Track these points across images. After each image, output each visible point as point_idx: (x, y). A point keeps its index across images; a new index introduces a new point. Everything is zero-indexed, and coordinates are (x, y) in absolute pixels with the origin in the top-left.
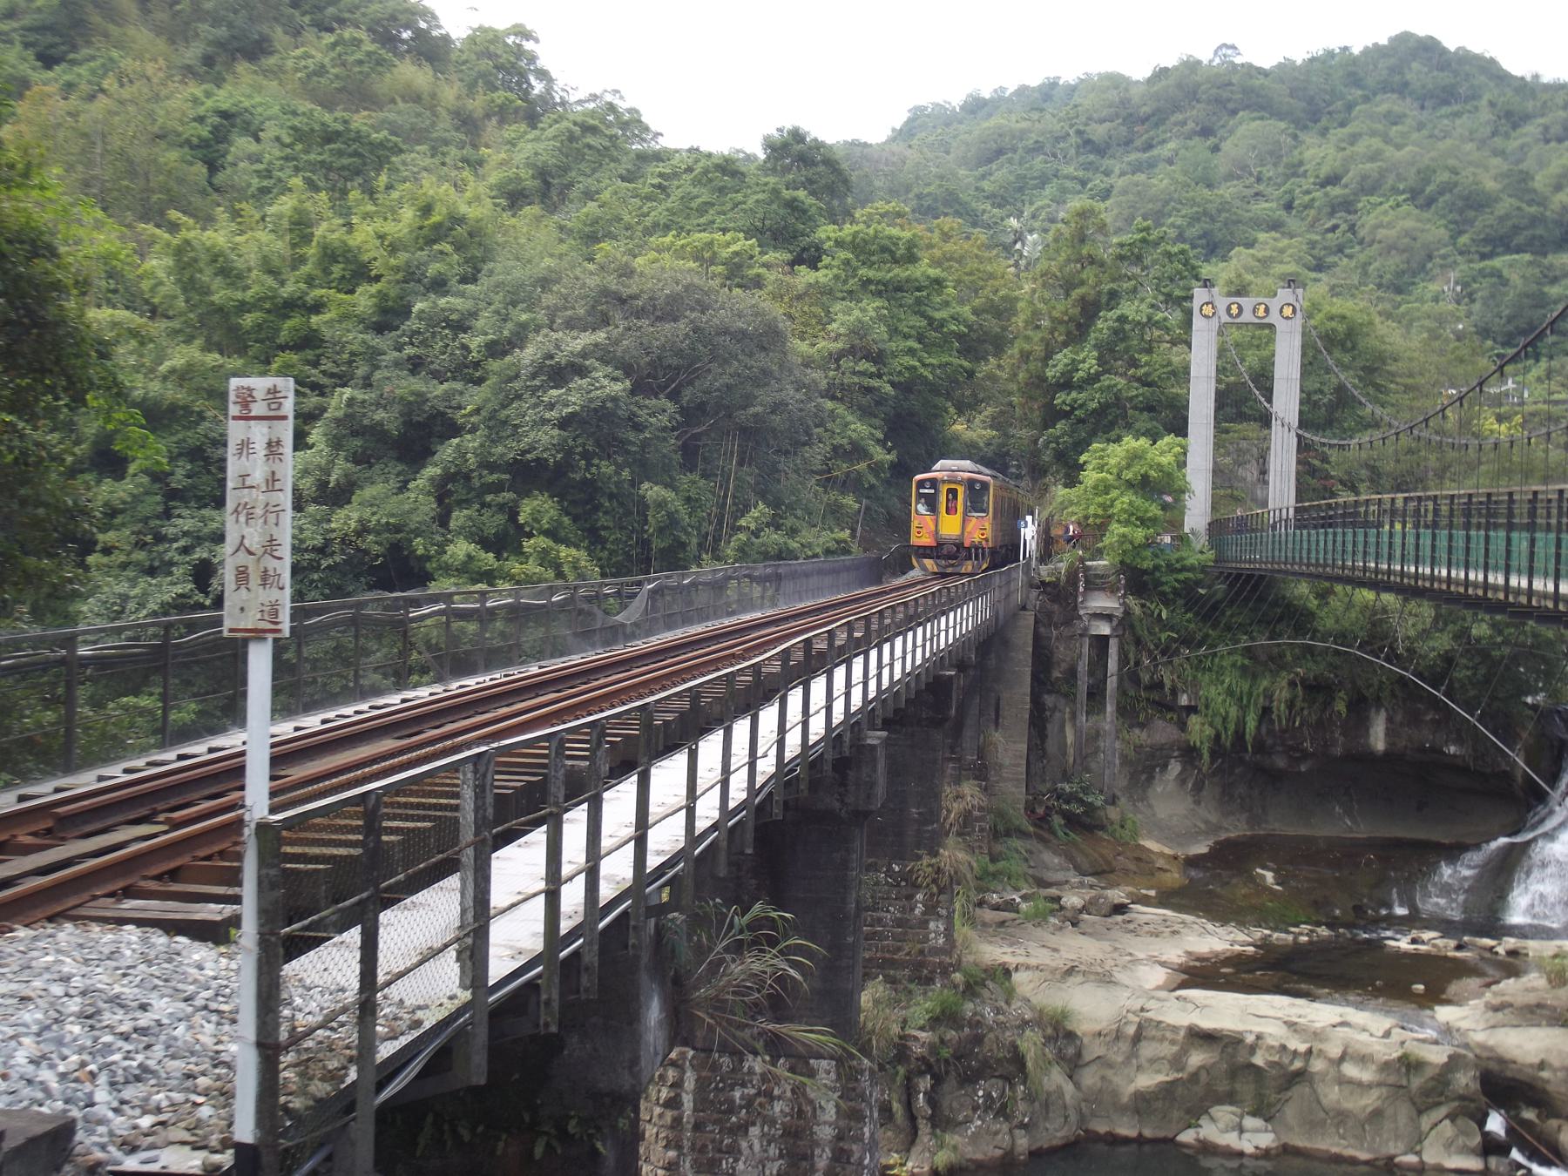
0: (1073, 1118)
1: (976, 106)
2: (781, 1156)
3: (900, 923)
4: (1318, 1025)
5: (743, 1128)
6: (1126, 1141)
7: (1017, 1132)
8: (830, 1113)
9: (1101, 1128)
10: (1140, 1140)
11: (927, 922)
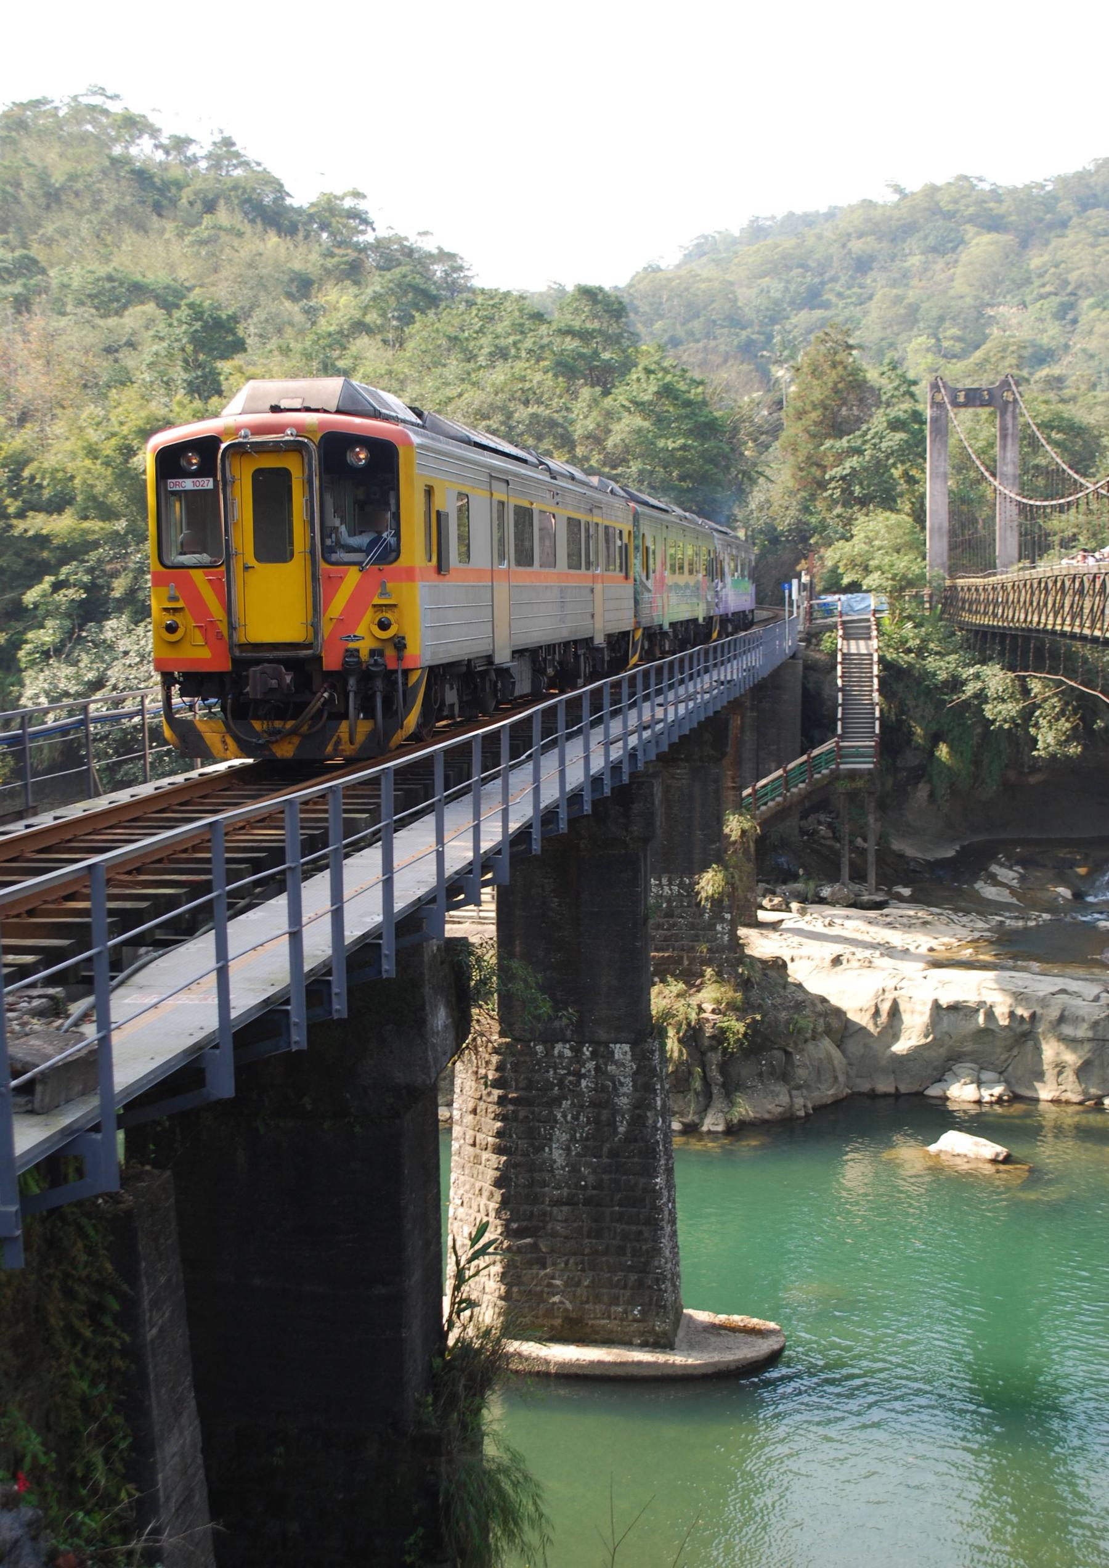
0: (842, 1079)
1: (757, 231)
2: (589, 1123)
3: (692, 926)
4: (1041, 994)
5: (557, 1101)
6: (886, 1095)
7: (795, 1092)
8: (628, 1087)
9: (864, 1086)
10: (897, 1095)
11: (715, 925)
